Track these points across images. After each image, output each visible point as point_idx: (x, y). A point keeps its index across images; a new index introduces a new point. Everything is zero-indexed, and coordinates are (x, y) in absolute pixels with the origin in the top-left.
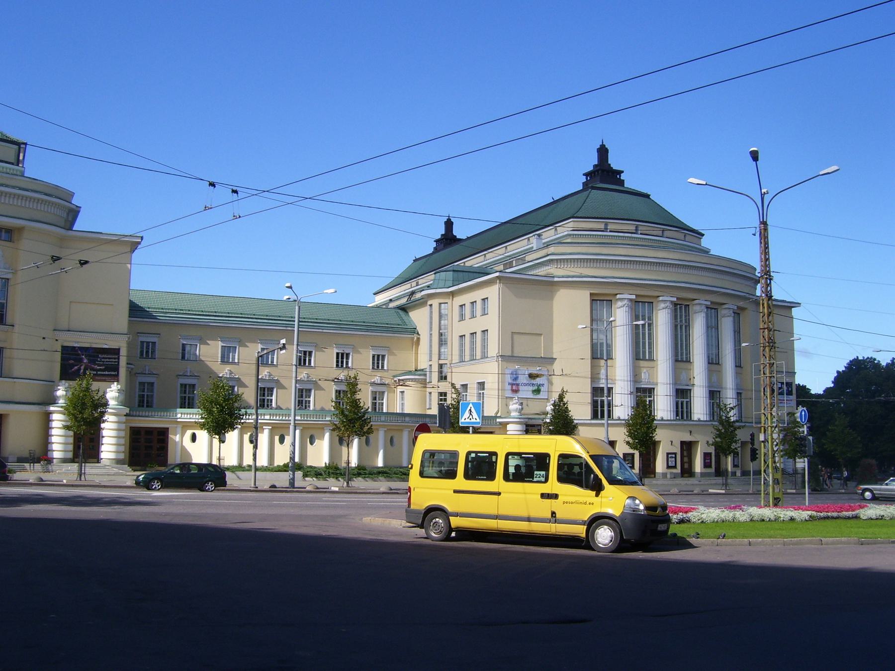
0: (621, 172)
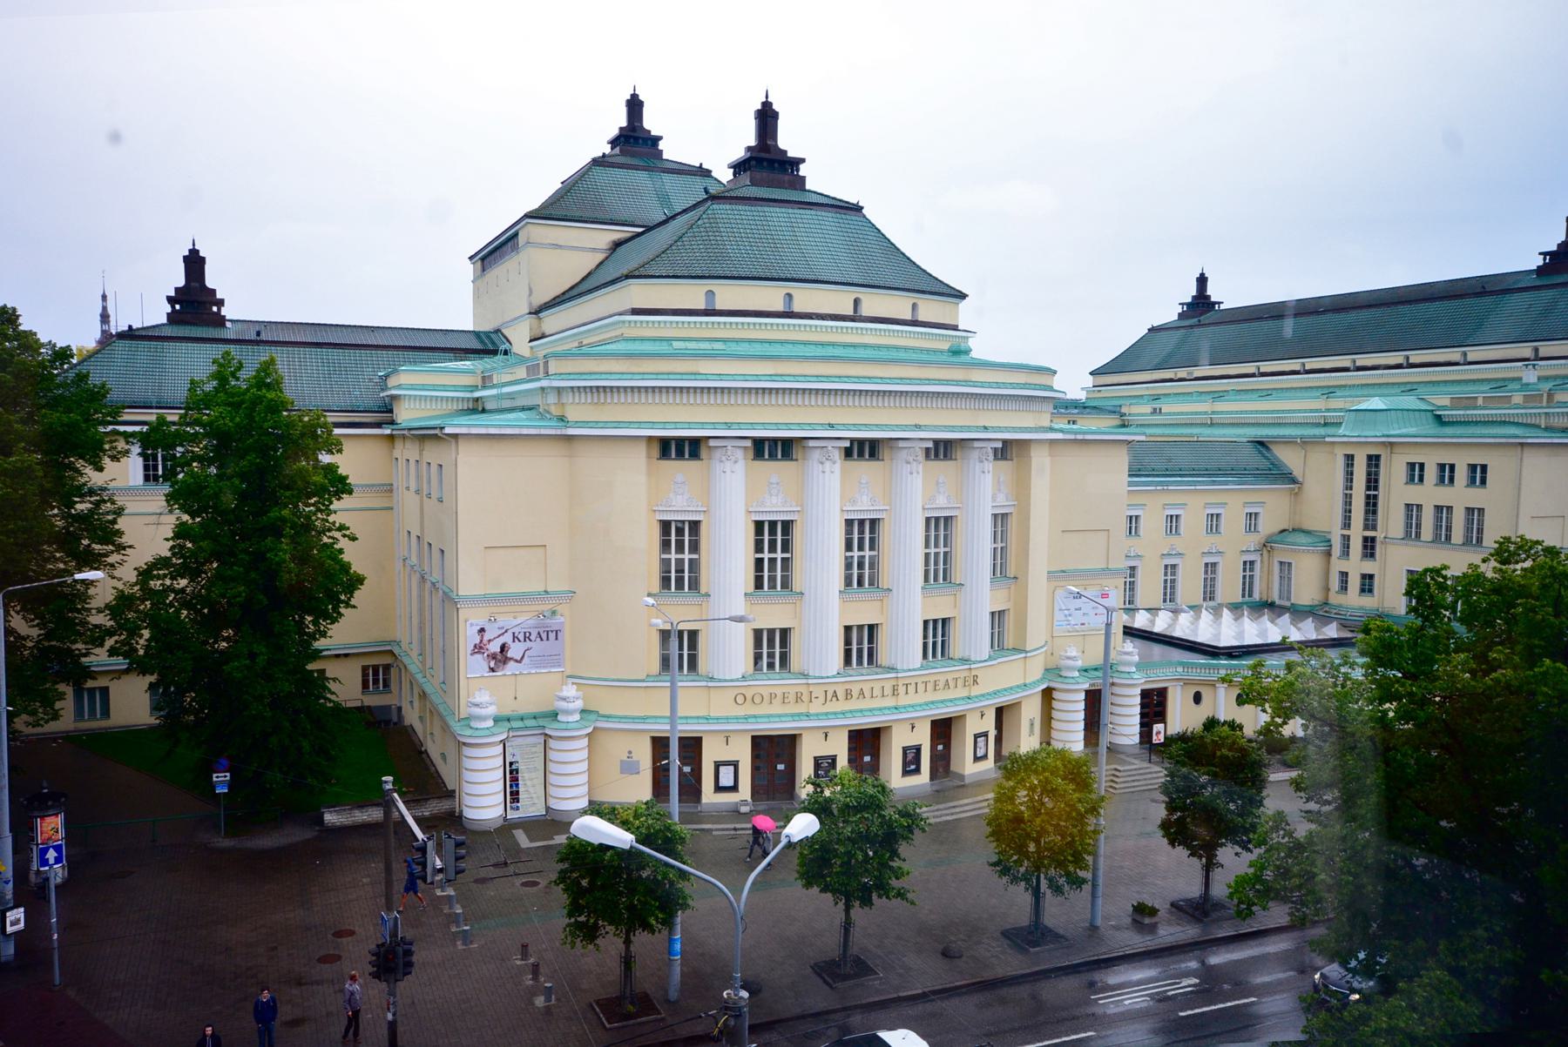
0: (660, 138)
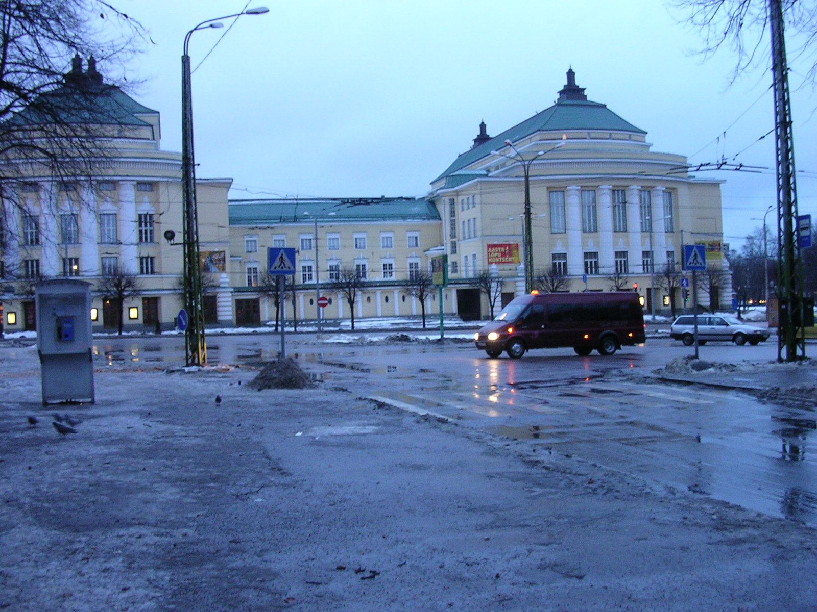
0: (584, 89)
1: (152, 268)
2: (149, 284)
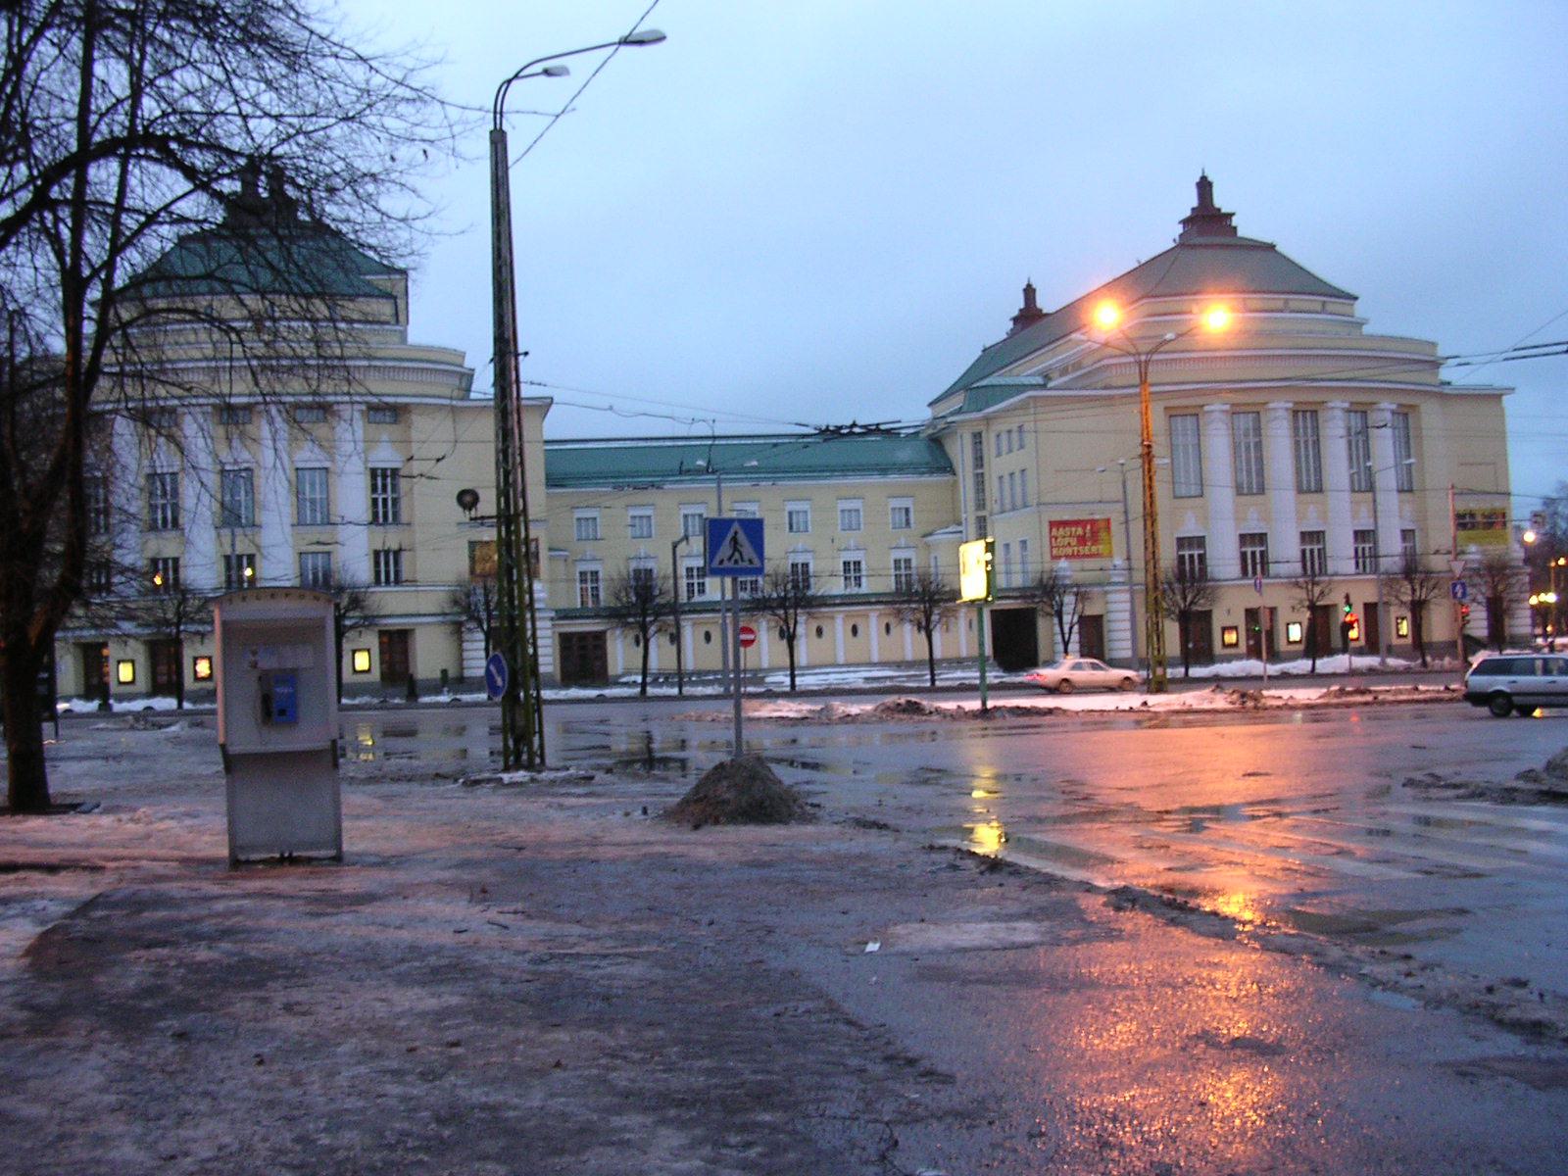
0: (1231, 215)
1: (397, 573)
2: (393, 603)
